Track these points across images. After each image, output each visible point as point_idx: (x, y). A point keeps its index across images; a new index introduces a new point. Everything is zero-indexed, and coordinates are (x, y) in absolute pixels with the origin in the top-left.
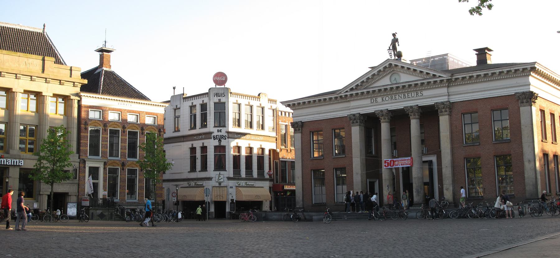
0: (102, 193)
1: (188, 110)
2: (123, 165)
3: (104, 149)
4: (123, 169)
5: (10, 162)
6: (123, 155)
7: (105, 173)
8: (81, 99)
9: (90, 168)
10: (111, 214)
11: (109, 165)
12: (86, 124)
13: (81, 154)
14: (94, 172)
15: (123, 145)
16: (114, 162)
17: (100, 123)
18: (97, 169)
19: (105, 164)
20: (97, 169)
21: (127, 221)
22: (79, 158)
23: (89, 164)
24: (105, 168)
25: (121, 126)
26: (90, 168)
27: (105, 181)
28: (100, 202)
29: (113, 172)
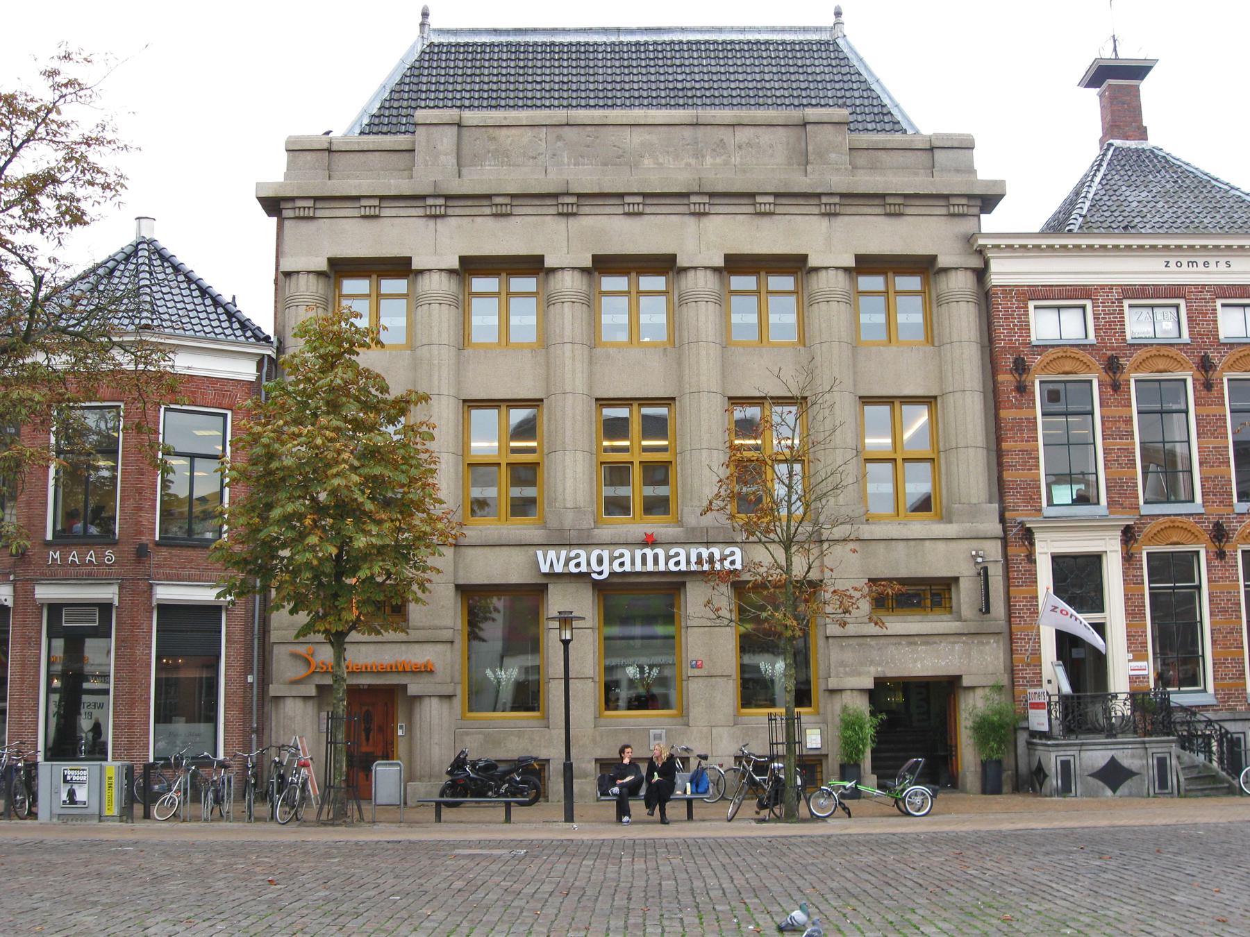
0: (1126, 669)
1: (920, 247)
2: (1219, 534)
3: (1212, 472)
4: (1221, 555)
5: (627, 559)
6: (1215, 490)
7: (1130, 580)
8: (987, 263)
9: (1056, 559)
10: (1162, 763)
11: (1152, 539)
12: (1020, 367)
13: (1010, 501)
14: (1079, 580)
15: (1212, 443)
16: (1173, 526)
17: (1087, 357)
18: (1094, 561)
19: (1128, 535)
20: (1094, 561)
21: (206, 820)
22: (1002, 520)
23: (1046, 548)
24: (1129, 559)
25: (1192, 361)
26: (1056, 559)
27: (1133, 612)
28: (1121, 708)
29: (1173, 568)
